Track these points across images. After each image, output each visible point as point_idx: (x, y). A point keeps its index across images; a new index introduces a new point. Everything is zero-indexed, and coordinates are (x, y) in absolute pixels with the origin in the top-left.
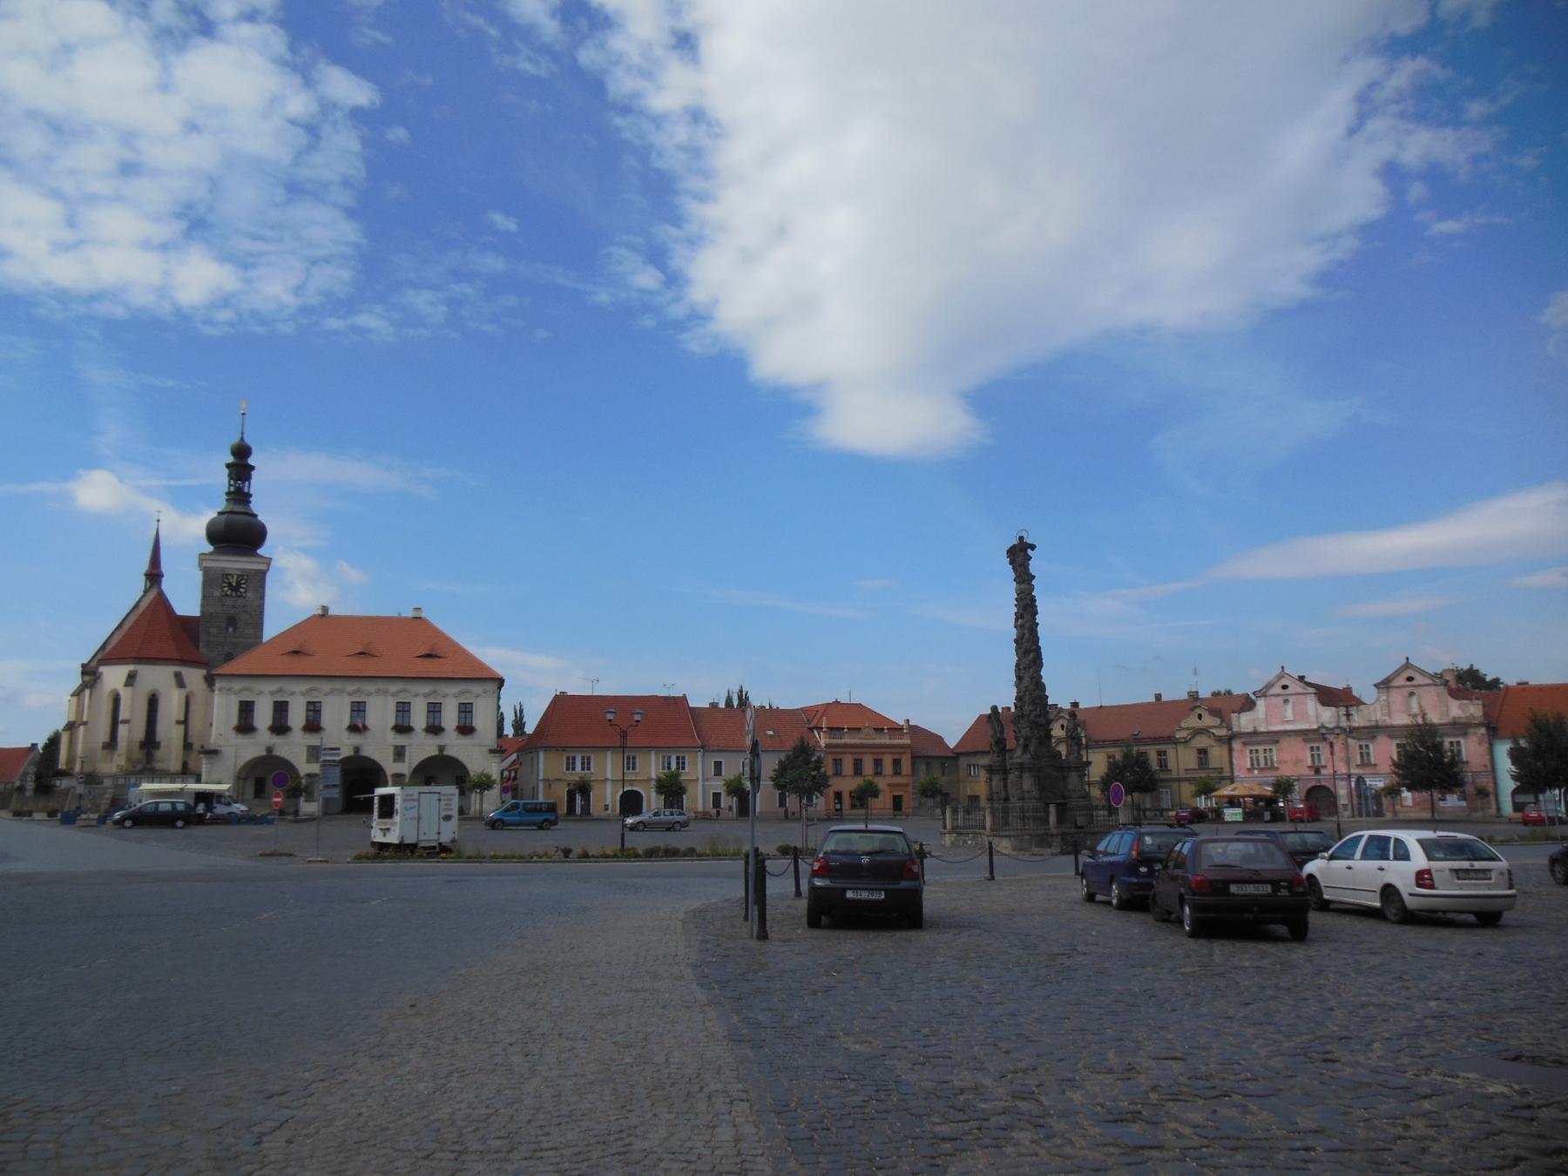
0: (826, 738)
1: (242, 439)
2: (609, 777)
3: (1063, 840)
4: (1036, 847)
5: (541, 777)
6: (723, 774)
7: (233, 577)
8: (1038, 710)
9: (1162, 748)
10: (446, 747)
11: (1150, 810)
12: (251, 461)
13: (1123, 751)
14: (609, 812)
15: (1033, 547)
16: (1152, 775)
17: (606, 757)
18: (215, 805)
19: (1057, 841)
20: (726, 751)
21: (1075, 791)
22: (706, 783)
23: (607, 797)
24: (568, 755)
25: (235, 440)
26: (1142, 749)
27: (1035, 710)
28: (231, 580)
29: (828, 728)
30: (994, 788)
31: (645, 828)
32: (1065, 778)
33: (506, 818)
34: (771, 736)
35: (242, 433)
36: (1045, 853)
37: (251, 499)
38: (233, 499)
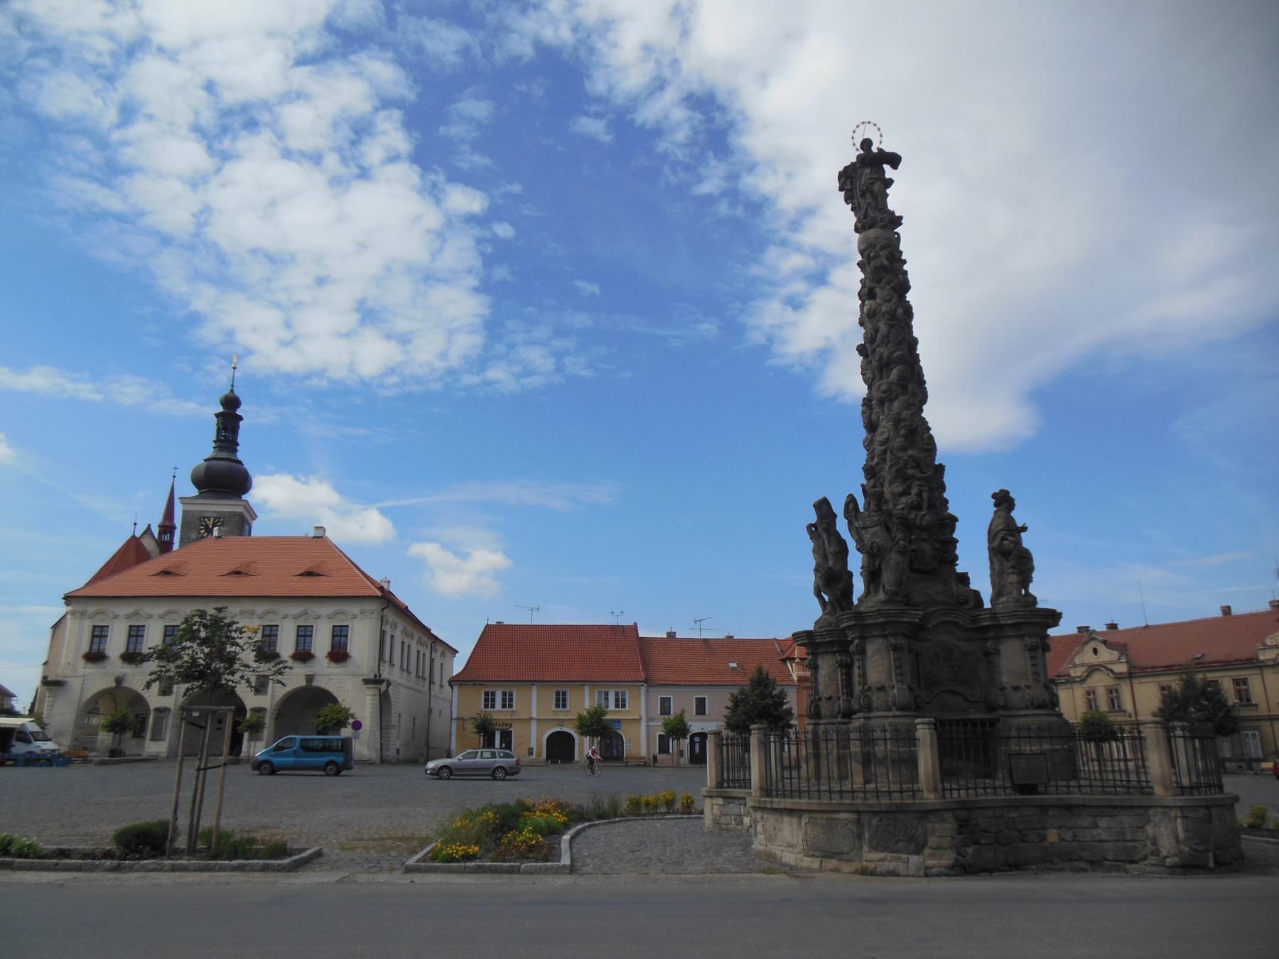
0: (798, 671)
1: (232, 391)
2: (534, 715)
3: (963, 826)
4: (875, 848)
5: (455, 716)
6: (707, 713)
7: (209, 520)
8: (914, 491)
9: (1241, 674)
10: (315, 677)
11: (1230, 760)
12: (239, 412)
13: (1181, 679)
14: (534, 757)
15: (894, 160)
16: (1228, 711)
17: (583, 696)
18: (14, 742)
19: (942, 831)
20: (674, 685)
21: (1017, 688)
22: (651, 724)
23: (534, 738)
24: (487, 690)
25: (227, 392)
26: (1211, 676)
27: (906, 492)
28: (208, 523)
29: (800, 659)
30: (821, 688)
31: (451, 774)
32: (990, 656)
33: (276, 760)
34: (733, 669)
35: (232, 386)
36: (901, 868)
37: (238, 448)
38: (219, 447)
